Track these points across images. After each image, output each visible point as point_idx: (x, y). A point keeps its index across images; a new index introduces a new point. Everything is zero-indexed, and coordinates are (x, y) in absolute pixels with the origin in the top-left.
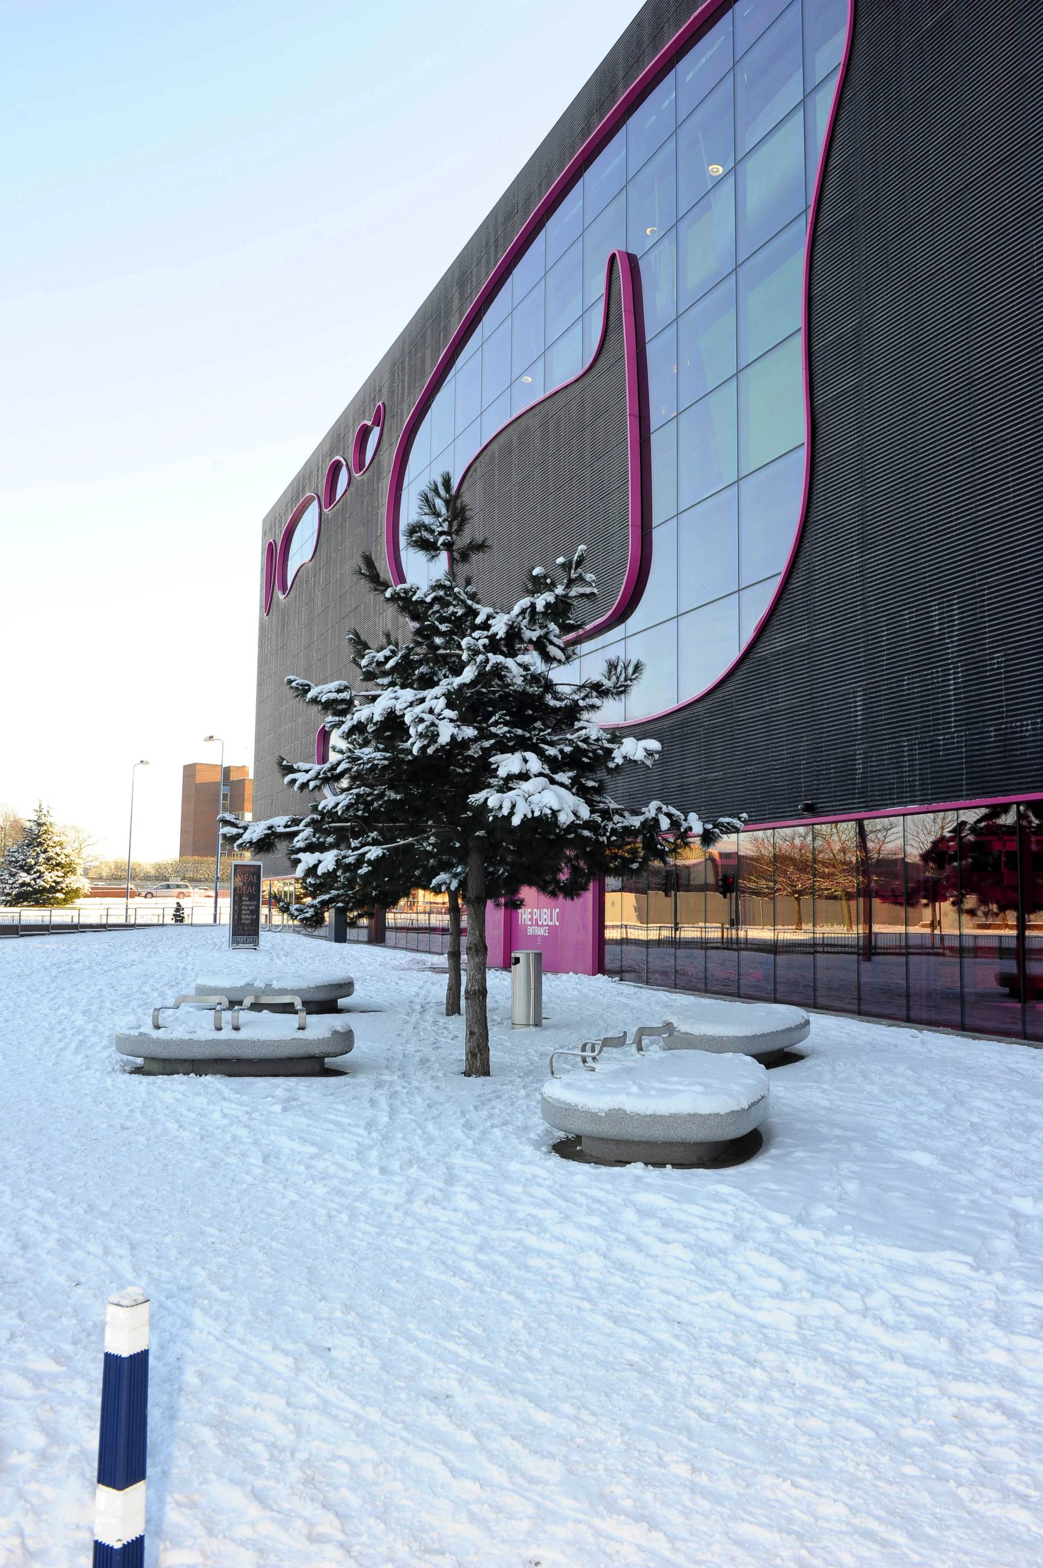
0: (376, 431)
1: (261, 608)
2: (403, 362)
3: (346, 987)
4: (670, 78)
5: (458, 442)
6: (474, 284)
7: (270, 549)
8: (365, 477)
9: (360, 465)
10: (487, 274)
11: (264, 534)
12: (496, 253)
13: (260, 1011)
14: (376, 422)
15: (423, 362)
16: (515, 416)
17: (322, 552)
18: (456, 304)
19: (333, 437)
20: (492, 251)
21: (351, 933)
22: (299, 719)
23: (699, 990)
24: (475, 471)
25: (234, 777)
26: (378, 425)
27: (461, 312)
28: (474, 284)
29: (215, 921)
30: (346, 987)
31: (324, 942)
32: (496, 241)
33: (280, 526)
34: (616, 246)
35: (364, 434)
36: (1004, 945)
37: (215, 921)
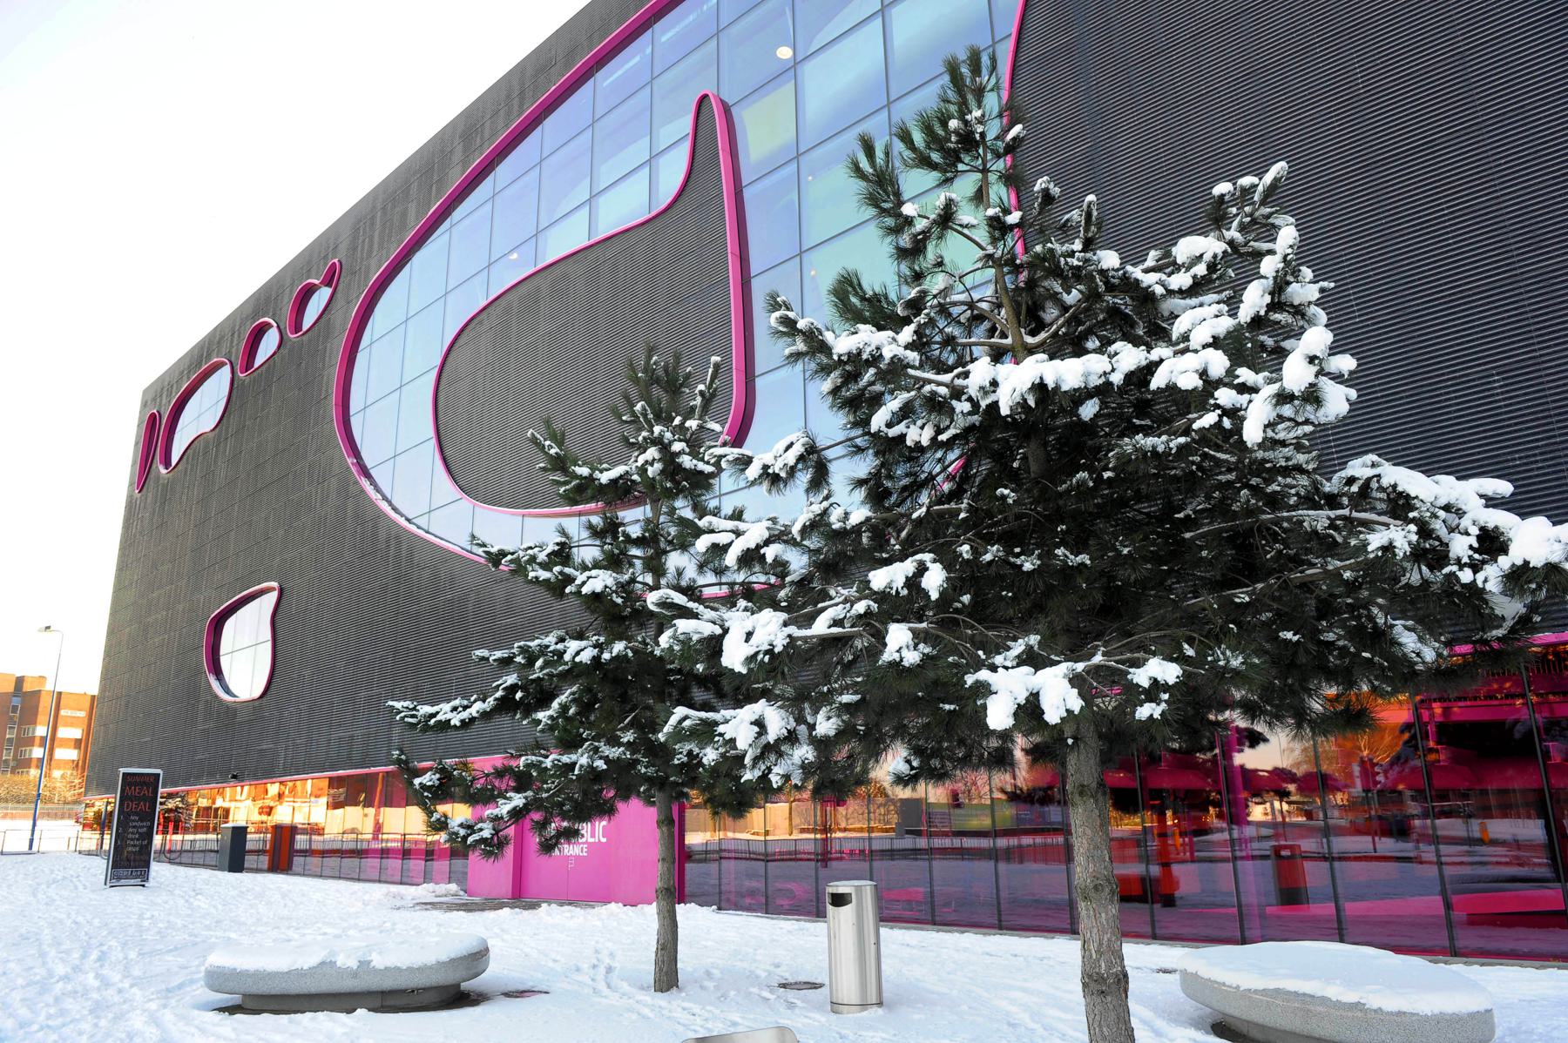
0: (324, 294)
1: (131, 484)
2: (373, 218)
3: (478, 958)
4: (647, 35)
5: (450, 298)
6: (487, 133)
7: (152, 422)
8: (305, 338)
9: (297, 327)
10: (507, 126)
11: (144, 405)
12: (521, 105)
13: (350, 1011)
14: (328, 282)
15: (404, 215)
16: (491, 298)
17: (233, 420)
18: (458, 156)
19: (258, 300)
20: (516, 102)
21: (250, 860)
22: (180, 608)
23: (808, 914)
24: (481, 323)
25: (27, 688)
26: (329, 284)
27: (465, 163)
28: (487, 133)
29: (31, 847)
30: (478, 958)
31: (260, 877)
32: (522, 93)
33: (170, 394)
34: (710, 89)
35: (307, 293)
36: (770, 850)
37: (31, 847)
